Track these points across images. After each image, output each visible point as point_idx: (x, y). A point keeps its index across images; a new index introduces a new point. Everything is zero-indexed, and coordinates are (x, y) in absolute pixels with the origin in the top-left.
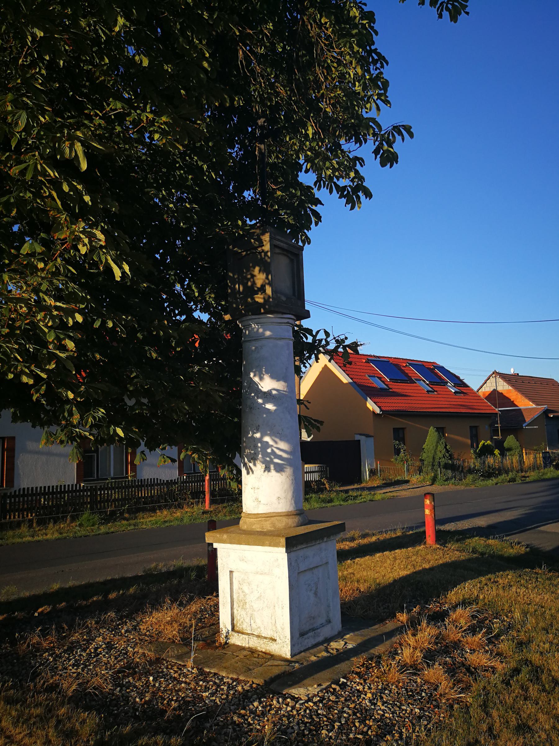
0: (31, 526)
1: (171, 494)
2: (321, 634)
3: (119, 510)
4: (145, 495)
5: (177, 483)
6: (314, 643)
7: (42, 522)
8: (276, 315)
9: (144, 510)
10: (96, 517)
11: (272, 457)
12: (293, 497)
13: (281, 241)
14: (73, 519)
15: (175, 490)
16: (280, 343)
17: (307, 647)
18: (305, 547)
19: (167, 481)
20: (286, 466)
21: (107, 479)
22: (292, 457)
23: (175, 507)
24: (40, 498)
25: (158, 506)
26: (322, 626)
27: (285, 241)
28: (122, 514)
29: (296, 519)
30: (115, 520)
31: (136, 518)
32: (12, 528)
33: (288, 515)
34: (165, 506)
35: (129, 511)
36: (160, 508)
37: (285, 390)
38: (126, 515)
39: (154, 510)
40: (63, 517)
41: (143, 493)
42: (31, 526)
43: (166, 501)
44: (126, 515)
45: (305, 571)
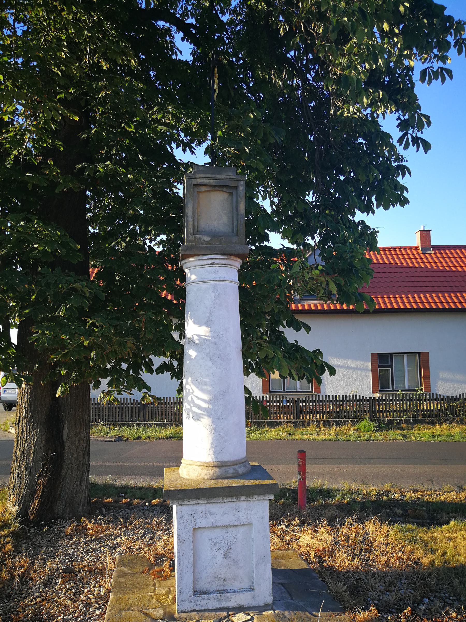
0: (318, 426)
1: (452, 409)
2: (232, 600)
3: (397, 420)
4: (430, 407)
5: (458, 399)
6: (218, 606)
7: (327, 424)
8: (196, 258)
9: (421, 422)
10: (373, 424)
11: (192, 405)
12: (212, 447)
13: (206, 178)
14: (354, 423)
15: (457, 406)
16: (204, 286)
17: (206, 608)
18: (203, 503)
19: (448, 397)
20: (204, 417)
21: (398, 391)
22: (211, 407)
23: (457, 422)
24: (330, 404)
25: (437, 420)
26: (240, 590)
27: (213, 176)
28: (399, 423)
29: (218, 471)
30: (390, 429)
31: (412, 428)
32: (303, 425)
33: (205, 465)
34: (445, 421)
35: (406, 422)
36: (440, 422)
37: (207, 335)
38: (403, 425)
39: (433, 423)
40: (345, 422)
41: (426, 406)
42: (318, 426)
43: (447, 415)
44: (403, 425)
45: (205, 528)
